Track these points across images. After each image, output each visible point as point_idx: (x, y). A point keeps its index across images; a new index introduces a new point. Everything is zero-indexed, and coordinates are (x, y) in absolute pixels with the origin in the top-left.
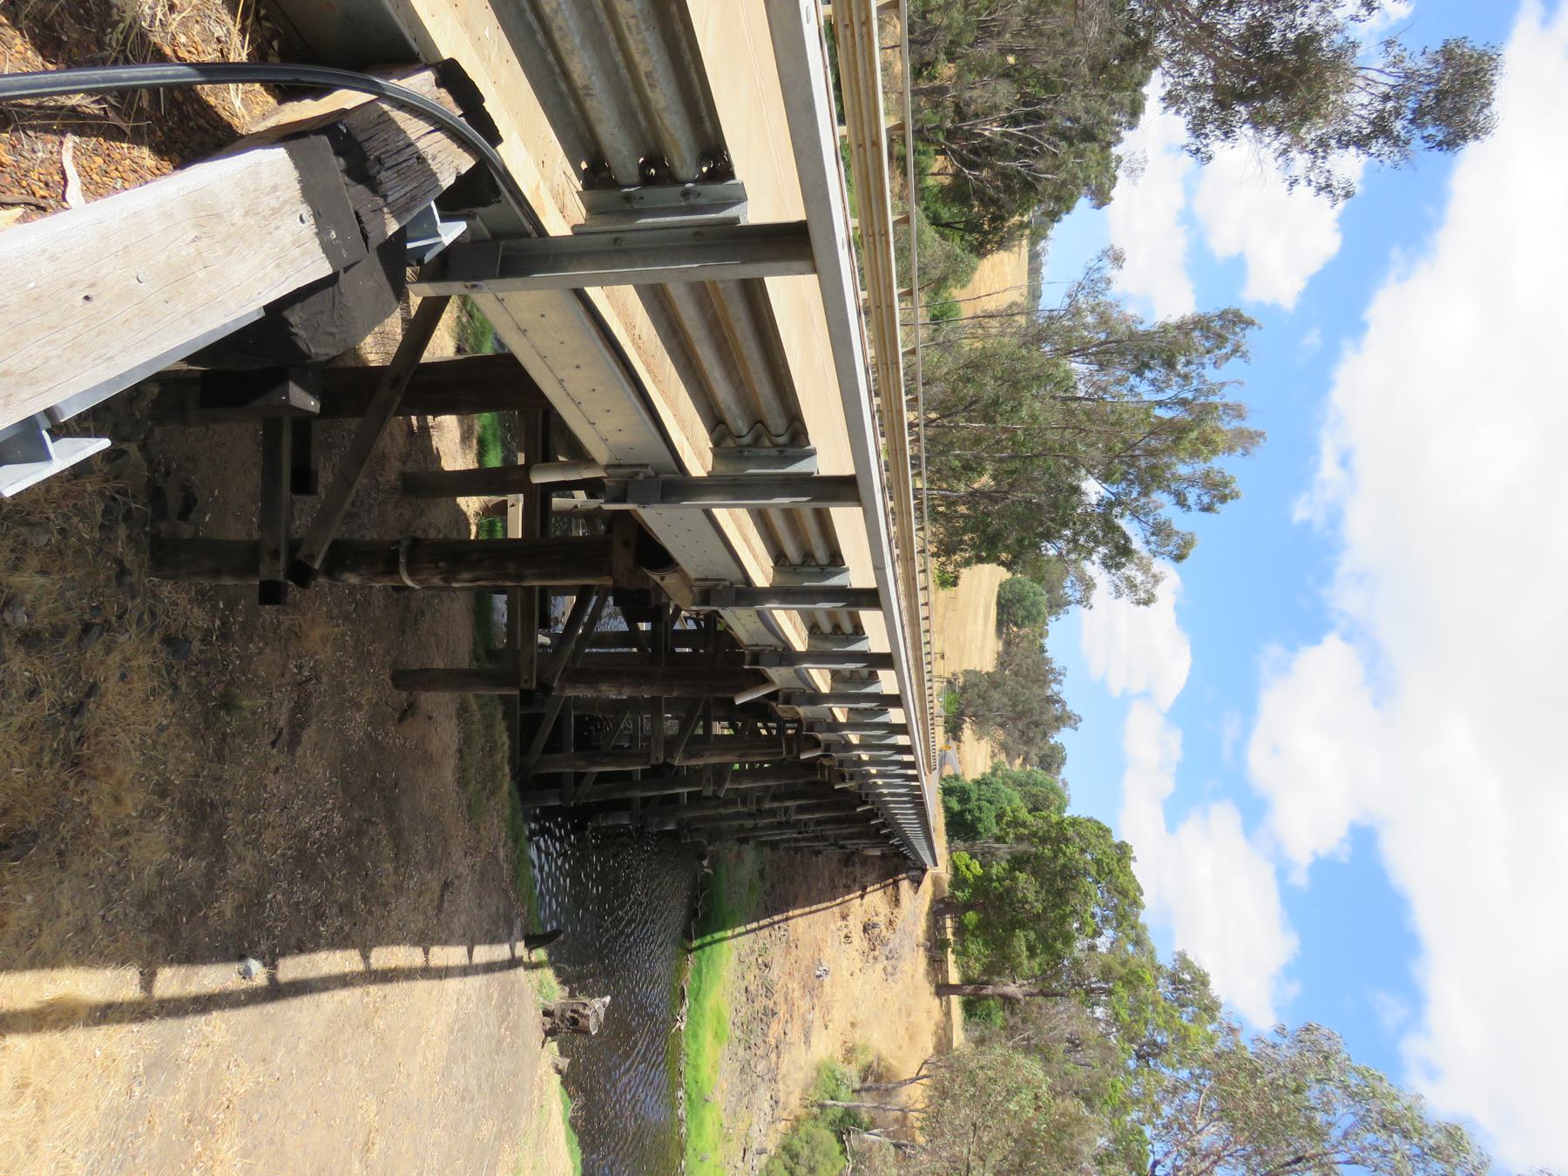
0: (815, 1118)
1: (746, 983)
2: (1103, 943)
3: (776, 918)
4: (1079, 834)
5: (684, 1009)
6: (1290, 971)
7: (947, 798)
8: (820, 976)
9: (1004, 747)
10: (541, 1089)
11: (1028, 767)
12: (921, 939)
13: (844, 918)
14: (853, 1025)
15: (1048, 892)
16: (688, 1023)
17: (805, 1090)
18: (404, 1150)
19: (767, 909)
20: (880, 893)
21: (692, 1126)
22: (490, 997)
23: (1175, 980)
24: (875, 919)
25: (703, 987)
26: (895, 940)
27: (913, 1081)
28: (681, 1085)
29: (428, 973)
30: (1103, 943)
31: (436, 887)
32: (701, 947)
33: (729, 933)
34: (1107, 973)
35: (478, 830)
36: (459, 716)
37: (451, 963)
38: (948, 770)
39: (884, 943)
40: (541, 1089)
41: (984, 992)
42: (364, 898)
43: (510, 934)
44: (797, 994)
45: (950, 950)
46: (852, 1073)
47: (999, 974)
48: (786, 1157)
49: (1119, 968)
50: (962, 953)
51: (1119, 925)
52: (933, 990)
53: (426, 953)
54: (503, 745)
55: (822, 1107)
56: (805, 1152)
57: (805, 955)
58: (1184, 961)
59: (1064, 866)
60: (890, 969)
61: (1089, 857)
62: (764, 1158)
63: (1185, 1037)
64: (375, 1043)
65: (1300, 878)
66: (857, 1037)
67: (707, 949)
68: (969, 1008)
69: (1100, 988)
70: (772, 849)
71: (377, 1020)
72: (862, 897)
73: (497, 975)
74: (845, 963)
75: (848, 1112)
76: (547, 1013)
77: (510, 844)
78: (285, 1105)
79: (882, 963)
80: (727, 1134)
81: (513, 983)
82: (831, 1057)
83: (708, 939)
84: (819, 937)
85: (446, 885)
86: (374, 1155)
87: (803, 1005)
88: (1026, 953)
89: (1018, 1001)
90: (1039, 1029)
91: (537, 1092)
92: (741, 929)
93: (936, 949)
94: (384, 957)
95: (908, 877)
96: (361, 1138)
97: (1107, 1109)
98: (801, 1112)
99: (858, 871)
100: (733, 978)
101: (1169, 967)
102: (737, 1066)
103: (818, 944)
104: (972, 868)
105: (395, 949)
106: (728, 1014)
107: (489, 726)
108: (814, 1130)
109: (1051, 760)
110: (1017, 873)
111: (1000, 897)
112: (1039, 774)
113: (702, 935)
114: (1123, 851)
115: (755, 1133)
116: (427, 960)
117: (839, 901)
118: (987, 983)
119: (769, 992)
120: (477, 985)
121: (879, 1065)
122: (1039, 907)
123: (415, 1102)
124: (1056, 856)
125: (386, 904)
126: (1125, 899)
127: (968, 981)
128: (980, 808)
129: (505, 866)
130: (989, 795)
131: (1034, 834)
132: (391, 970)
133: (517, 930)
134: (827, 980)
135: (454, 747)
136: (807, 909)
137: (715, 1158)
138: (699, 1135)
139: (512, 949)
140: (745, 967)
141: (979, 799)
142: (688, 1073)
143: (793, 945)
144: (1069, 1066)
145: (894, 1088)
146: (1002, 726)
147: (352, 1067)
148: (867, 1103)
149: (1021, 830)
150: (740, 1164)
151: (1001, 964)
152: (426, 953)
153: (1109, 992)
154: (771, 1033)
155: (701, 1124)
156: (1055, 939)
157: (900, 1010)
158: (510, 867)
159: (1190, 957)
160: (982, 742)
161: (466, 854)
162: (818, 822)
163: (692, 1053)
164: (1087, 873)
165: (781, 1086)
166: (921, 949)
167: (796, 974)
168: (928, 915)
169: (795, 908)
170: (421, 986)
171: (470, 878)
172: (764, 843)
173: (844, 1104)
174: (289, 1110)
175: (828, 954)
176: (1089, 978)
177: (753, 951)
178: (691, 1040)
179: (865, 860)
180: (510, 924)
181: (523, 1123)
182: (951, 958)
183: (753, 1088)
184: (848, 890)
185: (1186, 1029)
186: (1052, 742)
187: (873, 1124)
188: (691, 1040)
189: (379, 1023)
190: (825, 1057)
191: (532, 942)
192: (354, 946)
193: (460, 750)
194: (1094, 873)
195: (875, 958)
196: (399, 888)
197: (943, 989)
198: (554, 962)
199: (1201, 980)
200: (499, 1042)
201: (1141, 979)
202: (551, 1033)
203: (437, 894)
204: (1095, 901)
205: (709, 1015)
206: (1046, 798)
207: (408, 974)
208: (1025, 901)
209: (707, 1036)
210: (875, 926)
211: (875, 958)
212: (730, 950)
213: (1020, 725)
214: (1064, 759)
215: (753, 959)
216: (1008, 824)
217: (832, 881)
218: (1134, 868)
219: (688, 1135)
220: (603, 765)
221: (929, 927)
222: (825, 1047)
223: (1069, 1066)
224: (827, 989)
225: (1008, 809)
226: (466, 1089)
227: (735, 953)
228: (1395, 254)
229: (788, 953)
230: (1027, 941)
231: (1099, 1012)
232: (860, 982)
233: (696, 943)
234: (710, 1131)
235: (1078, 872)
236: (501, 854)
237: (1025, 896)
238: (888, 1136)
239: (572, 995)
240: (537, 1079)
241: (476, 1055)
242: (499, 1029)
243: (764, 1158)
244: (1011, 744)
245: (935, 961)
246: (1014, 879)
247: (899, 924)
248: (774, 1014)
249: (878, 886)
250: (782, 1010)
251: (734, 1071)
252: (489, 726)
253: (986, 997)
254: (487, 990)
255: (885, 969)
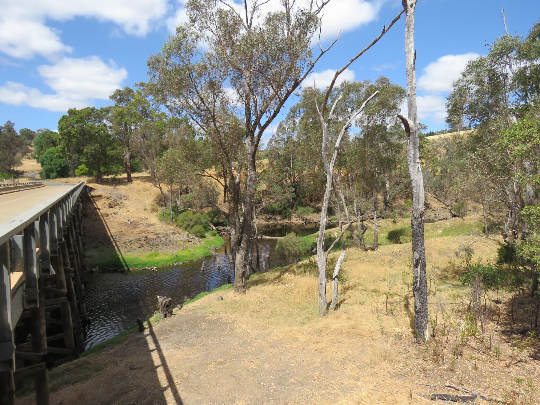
0: (176, 220)
1: (137, 248)
2: (108, 124)
3: (112, 240)
4: (66, 128)
5: (149, 268)
6: (106, 62)
7: (51, 177)
8: (131, 222)
9: (25, 154)
10: (188, 312)
11: (33, 144)
12: (113, 187)
13: (108, 215)
14: (145, 210)
15: (91, 141)
16: (154, 266)
17: (168, 224)
18: (218, 351)
19: (109, 244)
20: (97, 203)
21: (184, 259)
22: (165, 338)
23: (120, 101)
24: (107, 204)
25: (141, 263)
26: (114, 197)
27: (161, 190)
28: (173, 265)
29: (164, 363)
30: (108, 124)
31: (133, 372)
32: (127, 266)
33: (120, 256)
34: (119, 123)
35: (105, 365)
36: (56, 390)
37: (158, 356)
38: (38, 176)
39: (116, 200)
40: (188, 312)
41: (129, 166)
42: (145, 399)
43: (142, 338)
44: (138, 230)
45: (116, 177)
46: (160, 209)
47: (123, 160)
48: (189, 228)
49: (118, 119)
50: (116, 173)
51: (101, 117)
52: (130, 183)
53: (158, 367)
54: (65, 366)
55: (172, 218)
56: (186, 222)
57: (124, 228)
58: (113, 97)
59: (80, 134)
60: (125, 198)
61: (75, 125)
62: (190, 235)
63: (139, 100)
64: (191, 373)
65: (69, 49)
66: (149, 208)
67: (127, 264)
68: (134, 171)
69: (125, 127)
70: (85, 245)
71: (185, 376)
72: (99, 209)
73: (157, 338)
74: (125, 214)
75: (173, 210)
76: (165, 317)
77: (106, 348)
78: (217, 396)
79: (123, 200)
80: (185, 248)
81: (159, 332)
82: (156, 216)
83: (124, 264)
84: (116, 224)
85: (131, 369)
86: (222, 360)
87: (141, 228)
88: (115, 151)
89: (131, 154)
90: (141, 148)
91: (189, 313)
92: (118, 252)
93: (115, 182)
94: (163, 382)
95: (90, 192)
96: (219, 366)
97: (165, 129)
98: (175, 225)
99: (89, 211)
100: (136, 253)
101: (115, 102)
102: (164, 248)
103: (119, 224)
104: (81, 168)
105: (160, 379)
106: (149, 253)
107: (58, 375)
108: (180, 220)
109: (28, 134)
110: (84, 152)
111: (94, 159)
112: (36, 140)
113: (122, 267)
114: (72, 112)
115: (184, 239)
116: (160, 365)
117: (102, 218)
118: (126, 165)
119: (139, 240)
120: (163, 344)
121: (157, 201)
122: (97, 145)
123: (204, 352)
124: (76, 137)
125: (145, 389)
126: (90, 113)
127: (126, 171)
128: (55, 165)
129: (116, 348)
130: (48, 161)
131: (67, 144)
132: (167, 378)
133: (140, 336)
134: (132, 220)
135: (72, 387)
136: (107, 229)
137: (192, 250)
138: (187, 256)
139: (147, 335)
140: (131, 250)
141: (51, 165)
142: (170, 263)
143: (121, 233)
144: (152, 139)
145: (164, 196)
146: (14, 154)
147: (201, 378)
148: (170, 204)
149: (66, 150)
150: (193, 242)
151: (119, 160)
152: (158, 367)
153: (126, 124)
154: (153, 237)
155: (183, 256)
156: (109, 140)
157: (139, 194)
158: (115, 346)
159: (111, 94)
160: (23, 162)
161: (117, 365)
162: (75, 229)
163: (163, 263)
164: (82, 127)
165: (168, 232)
166: (116, 187)
167: (131, 231)
168: (103, 185)
169: (107, 234)
170: (169, 364)
171: (126, 360)
172: (84, 248)
173: (171, 211)
174: (218, 394)
175: (122, 220)
176: (122, 130)
177: (125, 247)
178: (159, 264)
179: (84, 209)
180: (139, 339)
181: (200, 315)
182: (118, 177)
183: (170, 241)
184: (97, 214)
185: (136, 100)
186: (19, 134)
187: (175, 202)
188: (159, 264)
189: (185, 374)
190: (157, 219)
191: (142, 329)
192: (163, 395)
193: (73, 384)
194: (82, 124)
195: (122, 203)
196: (138, 386)
197: (129, 180)
198: (147, 319)
199: (119, 92)
200: (179, 330)
201: (121, 112)
202: (171, 313)
203: (136, 371)
204: (89, 124)
205: (150, 259)
206: (48, 138)
207: (166, 370)
208: (95, 150)
209: (157, 259)
210: (110, 204)
211: (122, 203)
212: (126, 255)
213: (13, 146)
214: (27, 130)
215: (128, 247)
216: (64, 154)
217: (94, 221)
218: (79, 109)
219: (187, 260)
220: (69, 321)
221: (108, 185)
222: (154, 219)
223: (152, 139)
224: (135, 219)
225: (57, 154)
226: (195, 337)
227: (127, 253)
228: (61, 32)
229: (124, 234)
230: (111, 150)
231: (133, 128)
232: (130, 208)
233: (126, 268)
234: (185, 253)
235: (81, 130)
236: (112, 351)
237: (94, 150)
238: (178, 197)
239: (158, 309)
240: (186, 314)
241: (184, 337)
242: (174, 332)
243: (190, 235)
244: (23, 151)
245: (120, 182)
246: (87, 153)
247: (108, 195)
248: (146, 237)
249: (94, 204)
250: (144, 234)
251: (166, 248)
252: (58, 375)
253: (131, 165)
254: (163, 340)
255: (125, 200)
